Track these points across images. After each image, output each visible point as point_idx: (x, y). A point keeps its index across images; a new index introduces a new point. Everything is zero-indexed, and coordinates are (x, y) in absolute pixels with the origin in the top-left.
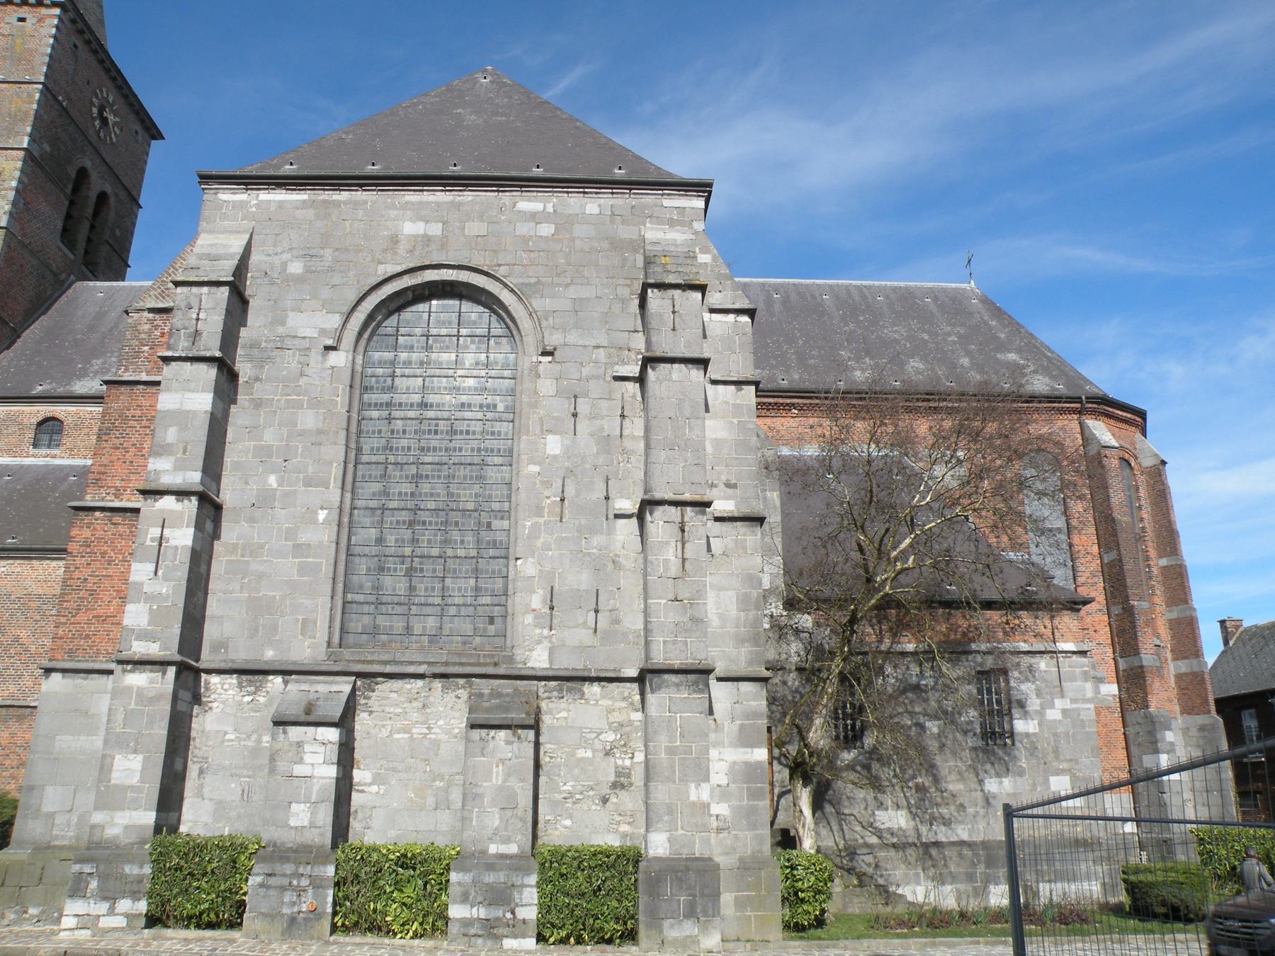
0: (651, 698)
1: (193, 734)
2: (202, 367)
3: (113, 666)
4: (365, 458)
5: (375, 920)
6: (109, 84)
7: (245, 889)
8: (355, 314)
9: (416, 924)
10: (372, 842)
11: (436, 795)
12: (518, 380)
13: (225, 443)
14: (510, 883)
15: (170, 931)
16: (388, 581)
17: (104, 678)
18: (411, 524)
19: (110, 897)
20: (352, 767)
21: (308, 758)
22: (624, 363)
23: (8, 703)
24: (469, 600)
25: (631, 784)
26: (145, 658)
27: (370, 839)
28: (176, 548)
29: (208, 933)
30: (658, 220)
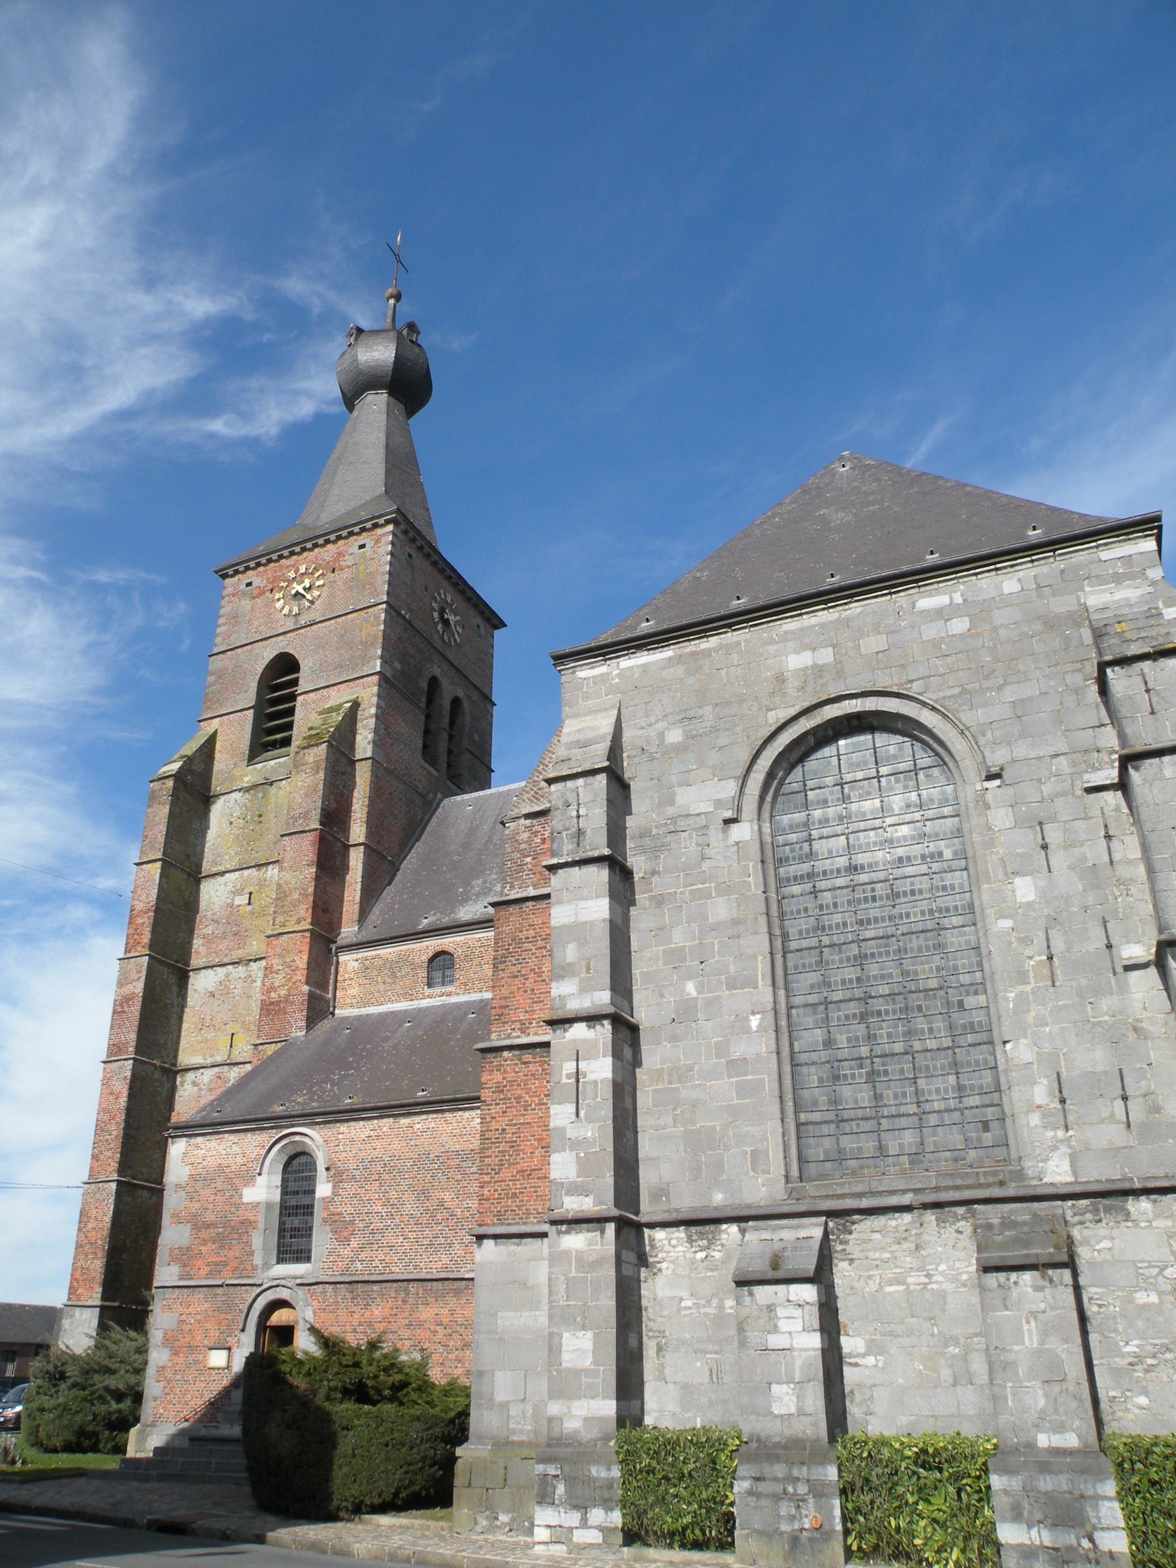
1: (644, 1303)
2: (592, 869)
3: (546, 1228)
4: (794, 945)
5: (900, 1543)
6: (446, 584)
7: (731, 1498)
10: (877, 1433)
12: (963, 816)
14: (1077, 1493)
16: (846, 1091)
17: (539, 1241)
18: (863, 1017)
19: (580, 1505)
20: (839, 1334)
21: (783, 1325)
22: (1095, 769)
23: (443, 1275)
24: (952, 1104)
26: (580, 1215)
27: (876, 1428)
28: (595, 1082)
29: (695, 1555)
30: (1101, 580)
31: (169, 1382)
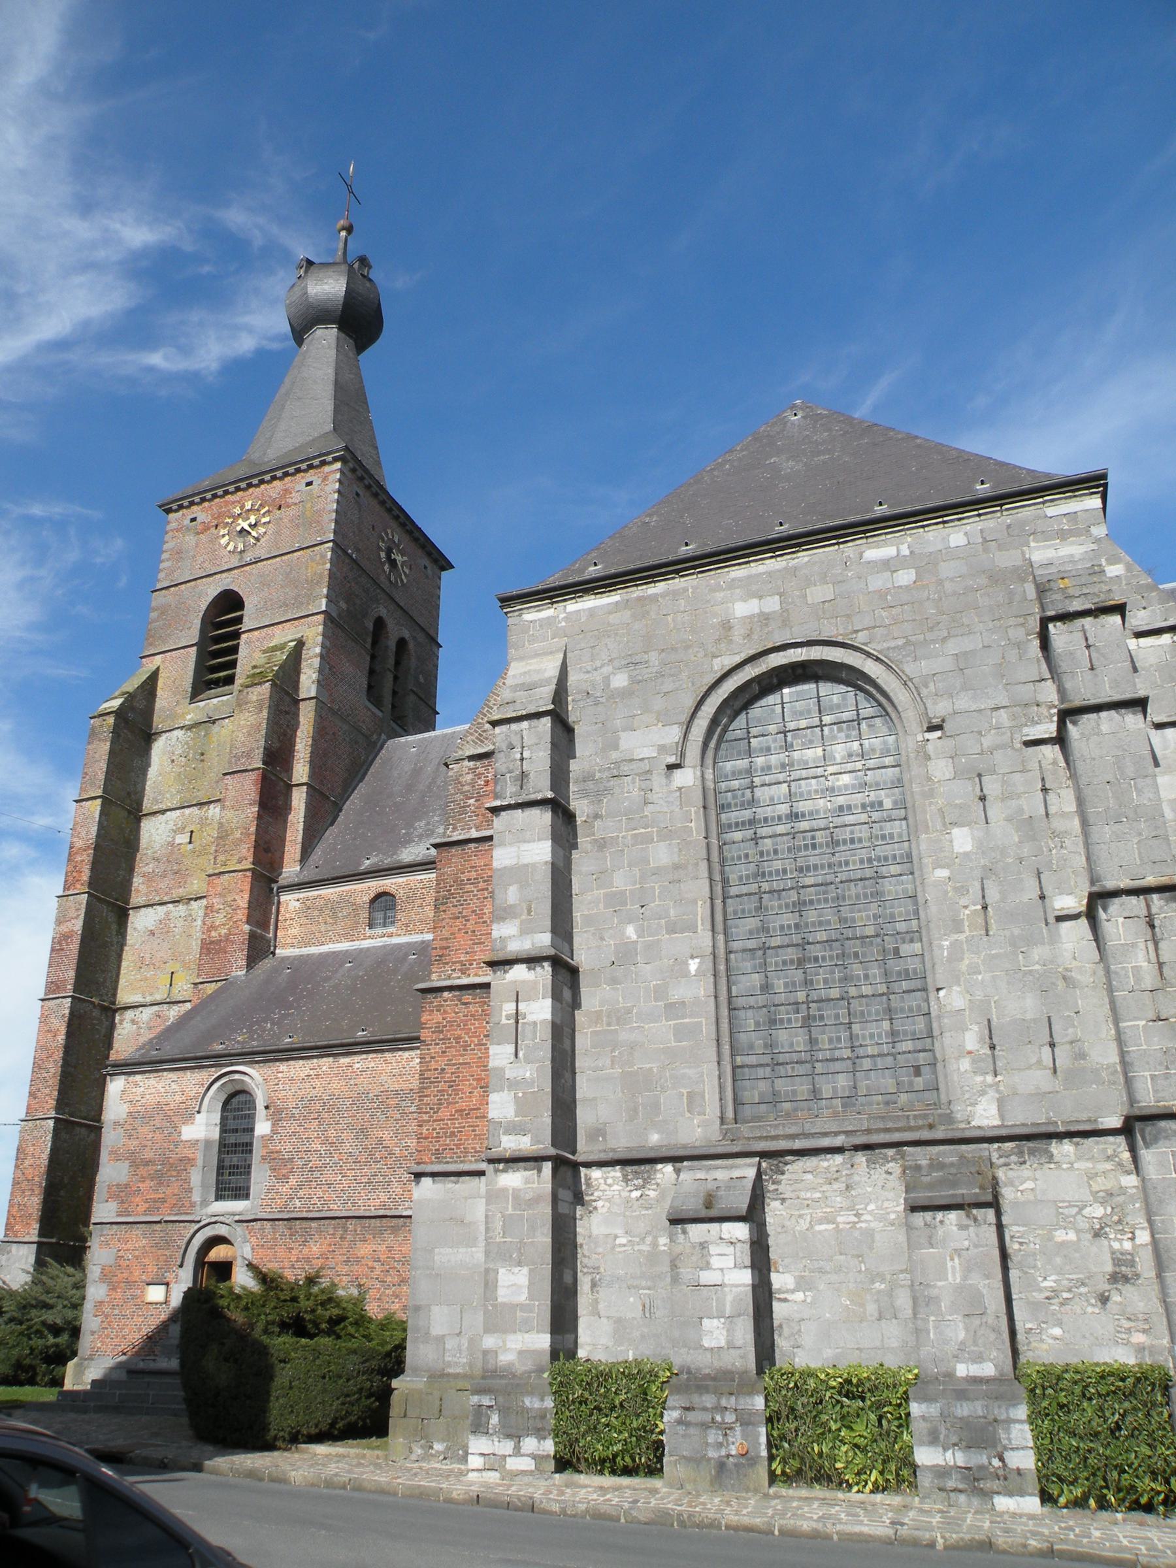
0: (1147, 1156)
1: (579, 1240)
2: (535, 812)
3: (483, 1166)
4: (734, 891)
5: (822, 1467)
6: (394, 524)
7: (661, 1426)
8: (696, 721)
9: (875, 1472)
10: (804, 1365)
11: (877, 1301)
12: (904, 766)
13: (571, 896)
14: (991, 1418)
15: (582, 1476)
16: (782, 1036)
18: (801, 962)
19: (514, 1435)
20: (769, 1270)
21: (716, 1262)
22: (1035, 723)
23: (381, 1213)
24: (885, 1049)
25: (1138, 1276)
26: (517, 1154)
27: (801, 1361)
28: (535, 1023)
29: (625, 1481)
30: (1045, 536)
31: (106, 1316)
